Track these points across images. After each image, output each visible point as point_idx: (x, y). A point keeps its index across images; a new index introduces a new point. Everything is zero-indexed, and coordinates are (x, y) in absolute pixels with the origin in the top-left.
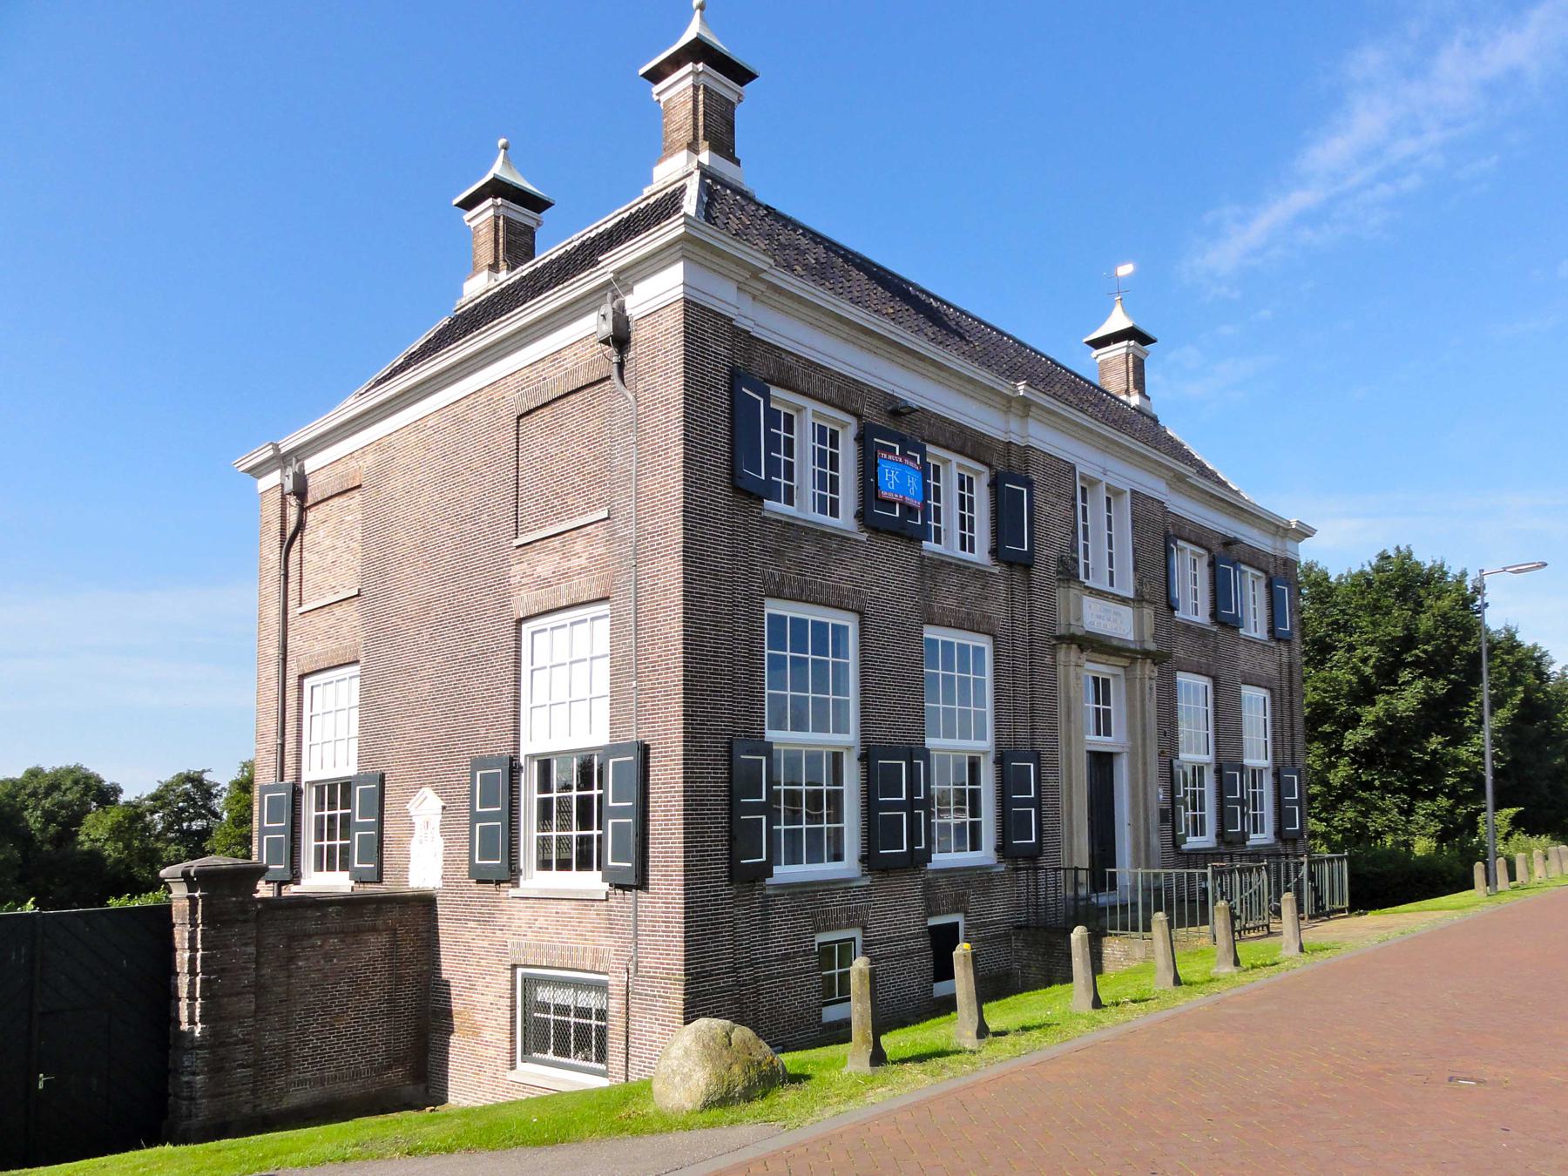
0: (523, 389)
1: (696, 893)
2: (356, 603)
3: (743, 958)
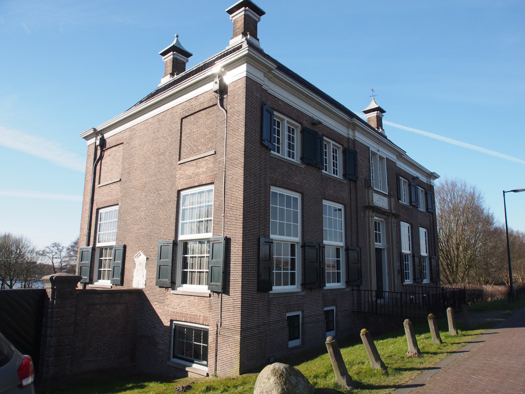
0: (184, 109)
1: (246, 296)
2: (119, 183)
3: (261, 322)
